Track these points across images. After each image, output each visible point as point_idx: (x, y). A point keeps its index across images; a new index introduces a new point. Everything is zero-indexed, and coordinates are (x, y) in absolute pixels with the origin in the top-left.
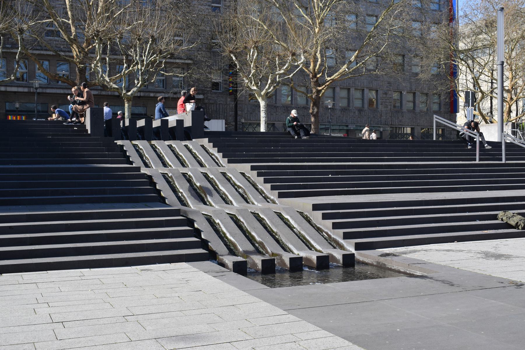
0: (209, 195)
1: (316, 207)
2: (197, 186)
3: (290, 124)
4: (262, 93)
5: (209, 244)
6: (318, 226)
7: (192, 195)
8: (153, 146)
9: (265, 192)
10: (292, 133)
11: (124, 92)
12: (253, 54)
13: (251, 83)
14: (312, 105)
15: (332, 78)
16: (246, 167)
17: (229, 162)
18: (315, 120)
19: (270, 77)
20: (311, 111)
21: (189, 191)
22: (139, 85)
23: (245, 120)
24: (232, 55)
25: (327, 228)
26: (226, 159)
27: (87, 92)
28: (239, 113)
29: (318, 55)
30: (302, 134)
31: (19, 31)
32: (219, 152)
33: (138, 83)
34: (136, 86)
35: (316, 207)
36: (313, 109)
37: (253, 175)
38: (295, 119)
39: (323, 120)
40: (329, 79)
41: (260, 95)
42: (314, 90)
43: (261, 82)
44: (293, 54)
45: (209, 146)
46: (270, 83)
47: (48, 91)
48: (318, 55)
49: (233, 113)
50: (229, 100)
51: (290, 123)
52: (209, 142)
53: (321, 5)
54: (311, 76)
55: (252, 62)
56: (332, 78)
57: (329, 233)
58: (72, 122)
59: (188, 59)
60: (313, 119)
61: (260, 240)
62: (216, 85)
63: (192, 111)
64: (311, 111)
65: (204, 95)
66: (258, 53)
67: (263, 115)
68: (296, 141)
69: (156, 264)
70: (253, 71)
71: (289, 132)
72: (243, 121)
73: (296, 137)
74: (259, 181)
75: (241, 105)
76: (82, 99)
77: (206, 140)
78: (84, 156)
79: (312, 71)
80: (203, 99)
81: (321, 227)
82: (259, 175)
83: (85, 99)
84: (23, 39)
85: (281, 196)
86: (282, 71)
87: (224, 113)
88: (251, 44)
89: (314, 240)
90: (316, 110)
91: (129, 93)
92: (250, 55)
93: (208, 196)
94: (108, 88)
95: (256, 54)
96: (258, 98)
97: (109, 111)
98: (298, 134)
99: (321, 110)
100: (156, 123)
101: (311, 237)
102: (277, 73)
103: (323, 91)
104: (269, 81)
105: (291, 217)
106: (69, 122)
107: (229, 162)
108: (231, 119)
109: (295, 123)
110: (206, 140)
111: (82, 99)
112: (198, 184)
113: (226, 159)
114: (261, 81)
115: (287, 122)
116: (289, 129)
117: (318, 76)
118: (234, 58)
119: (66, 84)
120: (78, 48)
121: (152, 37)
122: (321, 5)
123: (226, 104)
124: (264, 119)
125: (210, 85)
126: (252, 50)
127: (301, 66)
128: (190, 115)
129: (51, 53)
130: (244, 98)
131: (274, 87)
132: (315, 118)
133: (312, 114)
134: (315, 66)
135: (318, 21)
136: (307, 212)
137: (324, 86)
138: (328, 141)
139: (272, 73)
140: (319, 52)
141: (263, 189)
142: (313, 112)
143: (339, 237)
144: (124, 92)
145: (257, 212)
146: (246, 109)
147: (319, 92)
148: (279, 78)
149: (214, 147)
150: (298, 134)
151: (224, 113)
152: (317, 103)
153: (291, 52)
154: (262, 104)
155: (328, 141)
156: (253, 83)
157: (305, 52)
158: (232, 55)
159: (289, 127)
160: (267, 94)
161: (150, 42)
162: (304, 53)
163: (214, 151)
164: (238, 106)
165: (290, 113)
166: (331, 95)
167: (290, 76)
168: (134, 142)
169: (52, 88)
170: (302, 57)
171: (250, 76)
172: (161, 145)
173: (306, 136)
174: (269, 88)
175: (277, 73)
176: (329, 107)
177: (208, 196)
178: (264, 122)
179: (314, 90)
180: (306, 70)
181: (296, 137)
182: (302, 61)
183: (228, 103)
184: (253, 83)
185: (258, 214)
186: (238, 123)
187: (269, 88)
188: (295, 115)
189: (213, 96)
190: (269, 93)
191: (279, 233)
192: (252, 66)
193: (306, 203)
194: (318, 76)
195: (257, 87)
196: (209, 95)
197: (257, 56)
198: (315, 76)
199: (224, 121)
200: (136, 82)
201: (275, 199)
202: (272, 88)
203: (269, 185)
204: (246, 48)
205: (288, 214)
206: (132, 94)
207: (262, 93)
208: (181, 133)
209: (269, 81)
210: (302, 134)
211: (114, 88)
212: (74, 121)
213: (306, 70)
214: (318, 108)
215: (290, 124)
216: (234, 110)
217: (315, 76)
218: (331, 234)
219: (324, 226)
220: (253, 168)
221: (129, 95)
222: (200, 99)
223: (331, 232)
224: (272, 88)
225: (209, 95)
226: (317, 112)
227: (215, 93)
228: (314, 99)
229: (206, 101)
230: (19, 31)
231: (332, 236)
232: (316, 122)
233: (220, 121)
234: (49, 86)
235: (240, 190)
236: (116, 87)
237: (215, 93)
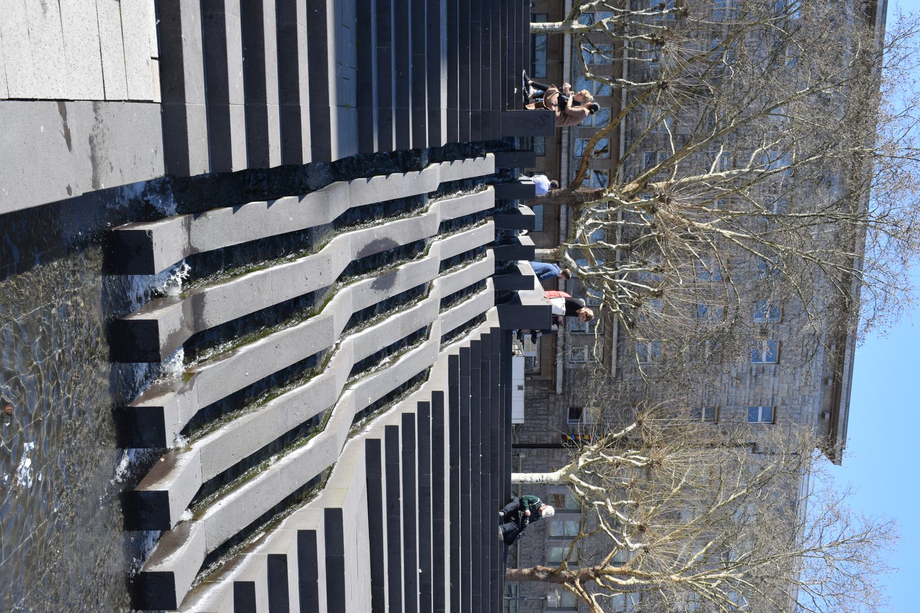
0: (375, 282)
1: (334, 518)
2: (400, 264)
3: (526, 502)
4: (572, 476)
5: (230, 209)
6: (284, 521)
7: (375, 242)
8: (479, 286)
9: (383, 415)
10: (510, 507)
11: (570, 246)
12: (637, 459)
13: (589, 457)
14: (550, 569)
15: (596, 603)
16: (440, 381)
17: (452, 358)
18: (524, 575)
19: (600, 489)
20: (539, 567)
21: (386, 240)
22: (580, 271)
23: (523, 460)
24: (634, 425)
25: (274, 542)
26: (457, 353)
27: (583, 111)
28: (534, 451)
29: (632, 581)
30: (509, 526)
31: (664, 83)
32: (472, 342)
33: (584, 270)
34: (579, 267)
35: (334, 518)
36: (542, 571)
37: (423, 393)
38: (536, 513)
39: (523, 589)
40: (594, 599)
41: (569, 472)
42: (574, 573)
43: (591, 475)
44: (642, 529)
45: (484, 328)
46: (590, 489)
47: (564, 156)
48: (632, 581)
49: (534, 442)
50: (555, 435)
51: (530, 502)
52: (492, 329)
53: (714, 585)
54: (598, 568)
55: (625, 457)
56: (596, 603)
57: (259, 548)
58: (527, 86)
59: (618, 370)
60: (526, 571)
61: (239, 353)
62: (576, 413)
63: (551, 306)
64: (539, 567)
65: (562, 394)
66: (642, 467)
67: (536, 477)
68: (494, 513)
69: (158, 16)
70: (610, 459)
71: (512, 500)
72: (522, 456)
73: (502, 514)
74: (409, 404)
75: (546, 454)
76: (570, 103)
77: (497, 324)
78: (464, 62)
79: (606, 569)
80: (555, 393)
81: (280, 528)
82: (422, 406)
83: (570, 108)
84: (649, 91)
85: (372, 446)
86: (611, 509)
87: (534, 428)
88: (654, 455)
89: (238, 500)
90: (541, 576)
91: (567, 256)
92: (635, 454)
93: (375, 279)
94: (576, 220)
95: (639, 464)
96: (564, 469)
97: (543, 190)
98: (506, 519)
99: (541, 586)
100: (526, 267)
101: (246, 494)
102: (608, 500)
103: (573, 589)
104: (593, 488)
105: (310, 451)
106: (526, 81)
107: (452, 358)
108: (524, 438)
109: (528, 512)
110: (497, 324)
111: (570, 103)
112: (401, 267)
113: (457, 353)
114: (591, 473)
115: (532, 497)
116: (516, 502)
117: (598, 580)
118: (630, 428)
119: (575, 175)
120: (634, 190)
121: (661, 292)
122: (714, 585)
123: (548, 431)
124: (529, 479)
125: (577, 404)
126: (645, 459)
127: (620, 543)
128: (544, 303)
129: (621, 156)
130: (558, 459)
131: (583, 497)
132: (528, 575)
133: (535, 569)
134: (611, 573)
135: (689, 579)
136: (323, 497)
137: (582, 590)
138: (494, 577)
139: (607, 492)
140: (637, 581)
141: (390, 412)
142: (538, 571)
143: (245, 572)
144: (570, 246)
145: (325, 371)
146: (540, 463)
147: (572, 581)
148: (599, 505)
149: (483, 335)
150: (506, 519)
151: (534, 428)
152: (553, 577)
153: (645, 524)
154: (554, 476)
155: (494, 577)
156: (590, 460)
157: (646, 550)
158: (634, 425)
159: (521, 501)
160: (571, 484)
161: (652, 290)
162: (645, 548)
163: (475, 334)
164: (545, 450)
165: (547, 504)
166: (565, 604)
167: (602, 525)
168: (490, 282)
169: (569, 162)
170: (637, 545)
171: (601, 454)
172: (487, 264)
173: (505, 534)
174: (581, 488)
175: (608, 500)
176: (549, 598)
177: (375, 279)
178: (523, 479)
179: (574, 573)
180: (606, 559)
181: (502, 514)
182: (631, 545)
183: (550, 433)
184: (590, 460)
185: (322, 372)
186: (518, 450)
187: (581, 488)
188: (544, 513)
189: (561, 410)
190: (573, 488)
191: (262, 410)
192: (618, 457)
193: (349, 492)
194: (598, 580)
195: (583, 467)
196: (562, 403)
197: (637, 467)
198: (598, 574)
199: (522, 422)
200: (585, 268)
201: (364, 434)
202: (582, 493)
203: (398, 422)
204: (649, 447)
205: (319, 445)
206: (566, 260)
207: (572, 476)
208: (508, 284)
209: (593, 488)
210: (509, 526)
211: (575, 231)
212: (528, 90)
213: (606, 559)
214: (545, 580)
215: (526, 502)
216: (539, 442)
217: (598, 574)
218: (255, 552)
219: (282, 534)
220: (437, 396)
221: (564, 254)
222: (555, 389)
223: (261, 551)
224: (582, 493)
225: (562, 403)
226: (538, 579)
227: (565, 413)
228: (560, 573)
229: (552, 398)
230: (664, 83)
231: (249, 555)
232: (521, 577)
233: (523, 416)
234: (571, 158)
235: (387, 359)
236: (578, 235)
237: (565, 413)
